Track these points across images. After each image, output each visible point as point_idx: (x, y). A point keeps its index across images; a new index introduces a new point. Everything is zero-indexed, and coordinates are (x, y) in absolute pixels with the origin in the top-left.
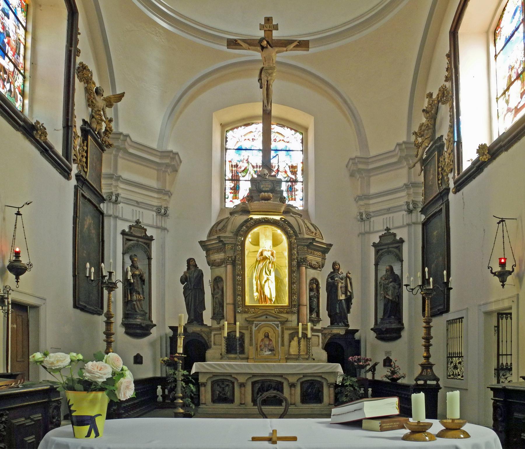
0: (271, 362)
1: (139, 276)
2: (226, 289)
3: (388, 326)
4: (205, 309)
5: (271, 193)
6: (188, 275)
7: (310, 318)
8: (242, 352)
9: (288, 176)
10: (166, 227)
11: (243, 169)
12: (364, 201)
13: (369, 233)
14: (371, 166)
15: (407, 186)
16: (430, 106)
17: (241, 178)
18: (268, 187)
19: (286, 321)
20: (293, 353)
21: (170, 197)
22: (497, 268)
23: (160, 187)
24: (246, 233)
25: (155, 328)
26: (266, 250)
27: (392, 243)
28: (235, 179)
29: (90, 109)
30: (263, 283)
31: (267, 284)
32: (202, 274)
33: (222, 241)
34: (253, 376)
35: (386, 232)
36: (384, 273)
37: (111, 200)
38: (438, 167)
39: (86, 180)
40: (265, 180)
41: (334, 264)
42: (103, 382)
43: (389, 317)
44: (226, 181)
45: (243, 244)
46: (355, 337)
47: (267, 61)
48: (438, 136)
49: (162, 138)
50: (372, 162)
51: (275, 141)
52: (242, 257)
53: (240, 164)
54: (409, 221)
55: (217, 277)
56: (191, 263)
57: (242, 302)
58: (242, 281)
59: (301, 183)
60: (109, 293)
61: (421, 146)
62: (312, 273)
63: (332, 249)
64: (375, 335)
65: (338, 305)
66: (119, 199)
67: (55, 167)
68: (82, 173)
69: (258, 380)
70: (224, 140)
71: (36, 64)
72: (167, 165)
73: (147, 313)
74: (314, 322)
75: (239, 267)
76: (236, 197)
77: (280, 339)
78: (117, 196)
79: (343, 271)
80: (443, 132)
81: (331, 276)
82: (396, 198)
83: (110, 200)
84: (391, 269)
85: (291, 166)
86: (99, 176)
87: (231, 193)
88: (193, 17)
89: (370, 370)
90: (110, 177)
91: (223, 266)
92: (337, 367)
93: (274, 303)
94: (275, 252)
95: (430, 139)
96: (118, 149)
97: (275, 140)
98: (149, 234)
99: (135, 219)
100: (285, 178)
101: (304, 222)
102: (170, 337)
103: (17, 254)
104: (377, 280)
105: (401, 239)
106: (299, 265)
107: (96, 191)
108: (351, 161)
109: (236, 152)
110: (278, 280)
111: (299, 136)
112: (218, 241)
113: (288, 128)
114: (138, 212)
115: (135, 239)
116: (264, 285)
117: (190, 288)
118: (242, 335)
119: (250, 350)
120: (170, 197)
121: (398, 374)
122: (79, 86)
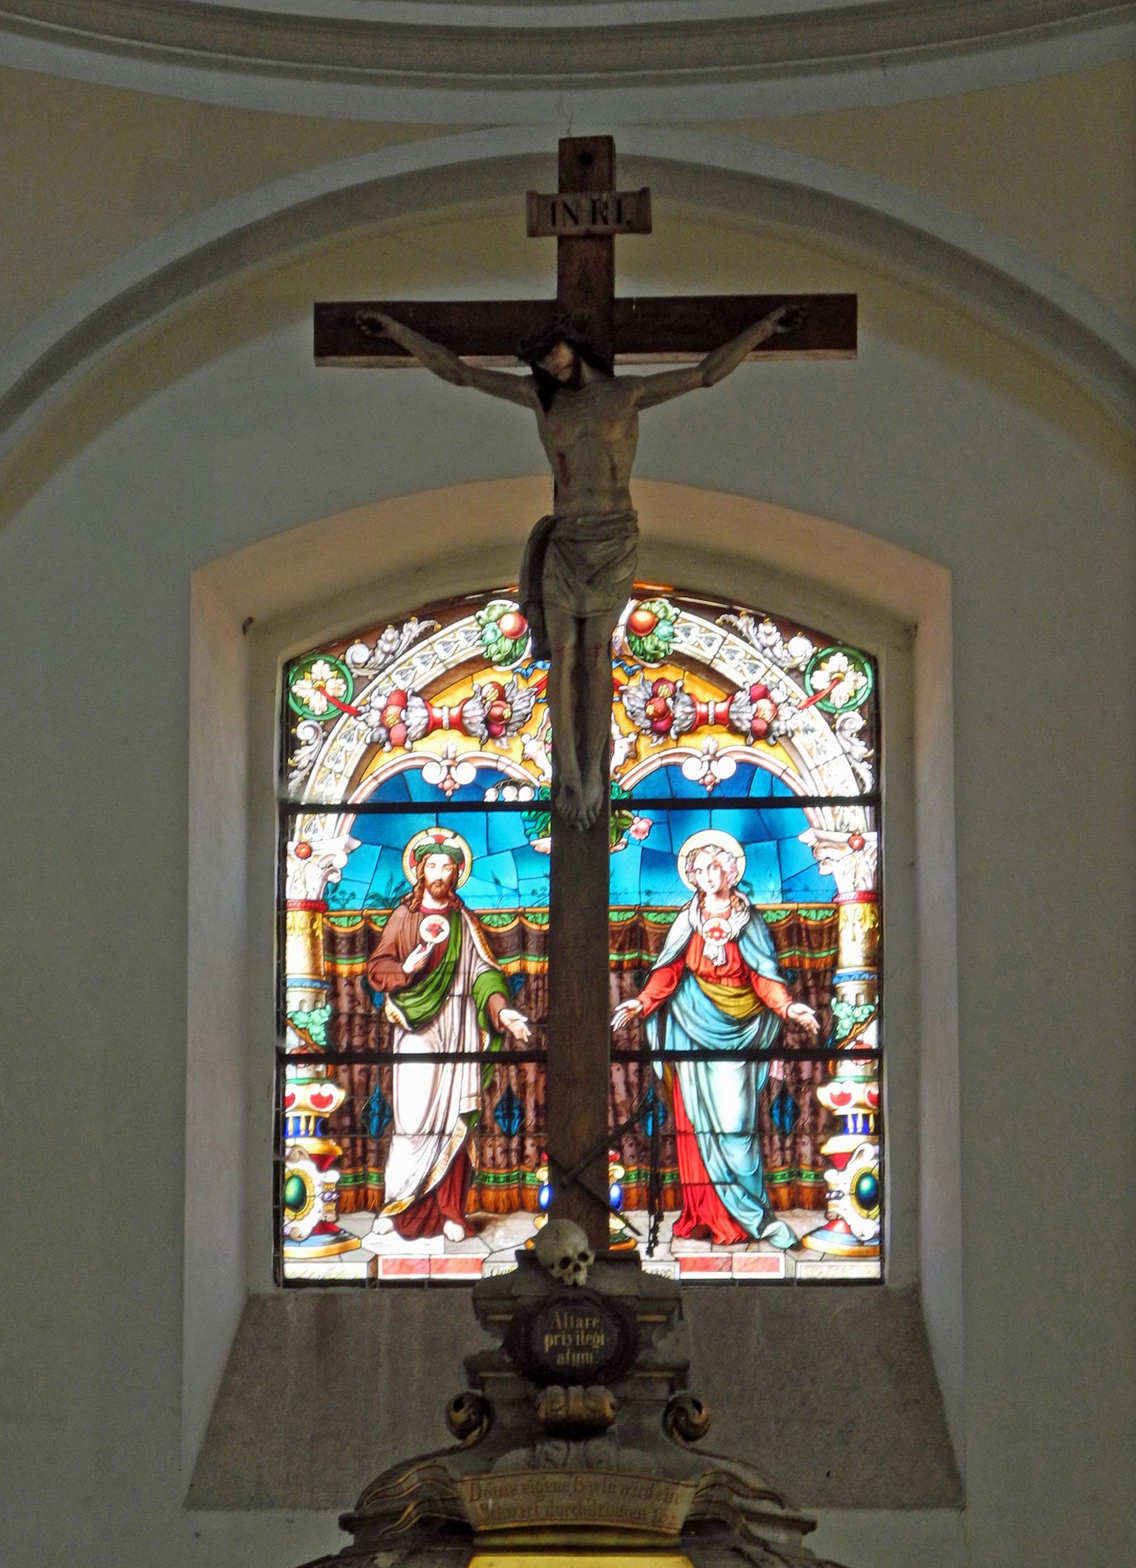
9: (764, 1009)
11: (413, 962)
18: (588, 1348)
40: (571, 1294)
51: (665, 733)
85: (789, 929)
100: (742, 1023)
113: (758, 620)
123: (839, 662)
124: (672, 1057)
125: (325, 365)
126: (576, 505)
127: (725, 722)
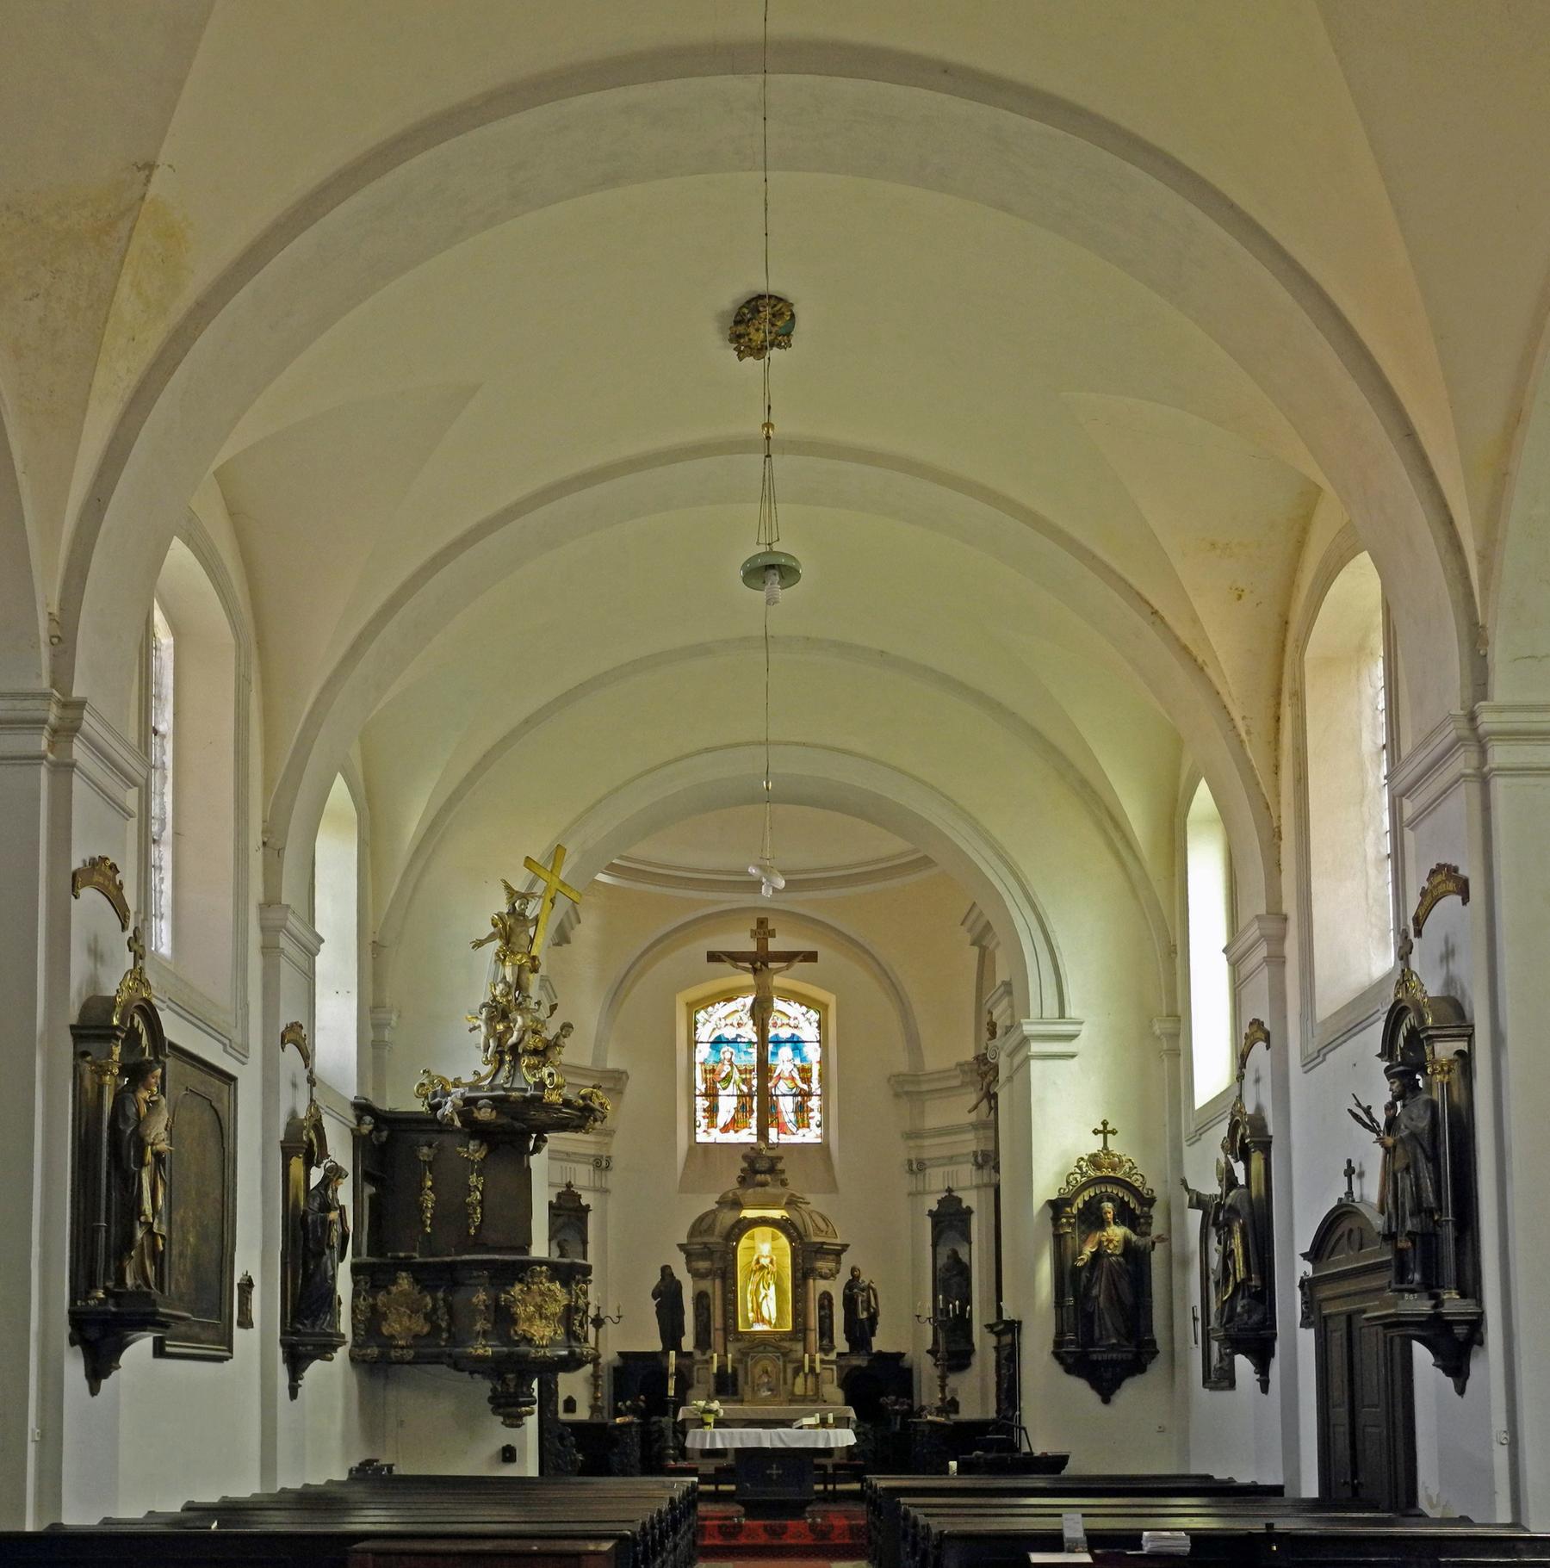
4: (684, 1334)
8: (735, 1393)
9: (797, 1086)
11: (723, 1075)
14: (925, 1087)
17: (721, 1092)
28: (711, 1094)
30: (760, 1300)
31: (765, 1301)
36: (945, 1260)
41: (853, 1270)
56: (666, 1271)
59: (817, 1098)
60: (597, 1331)
62: (821, 1285)
70: (693, 1026)
76: (712, 1125)
77: (782, 1375)
84: (955, 1253)
93: (775, 1327)
94: (775, 1258)
97: (775, 1025)
106: (805, 1277)
111: (813, 1016)
118: (735, 1370)
119: (746, 1391)
123: (812, 1012)
124: (777, 1096)
127: (788, 1024)
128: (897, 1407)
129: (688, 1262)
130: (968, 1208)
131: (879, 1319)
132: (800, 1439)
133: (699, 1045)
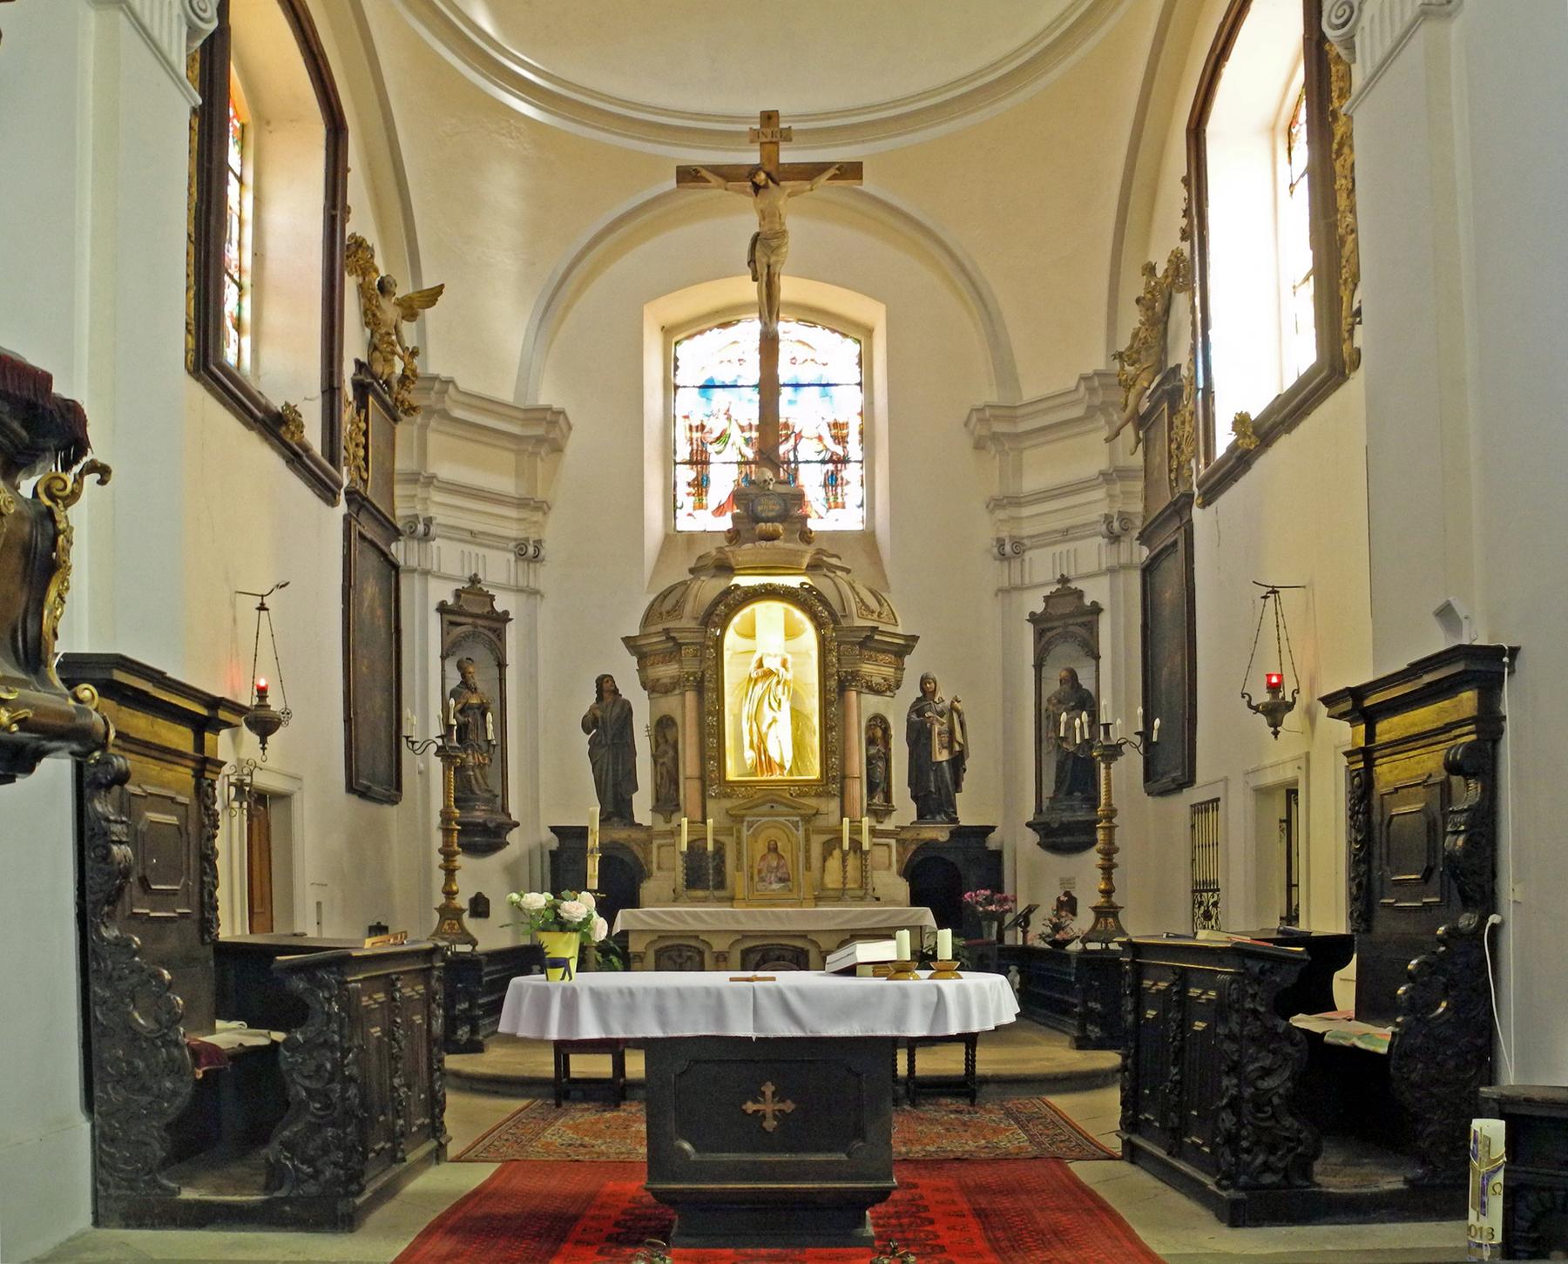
0: (782, 906)
1: (478, 708)
2: (684, 743)
3: (1067, 817)
4: (636, 789)
5: (781, 522)
6: (599, 713)
7: (868, 805)
8: (721, 885)
10: (537, 587)
11: (716, 434)
12: (1007, 511)
13: (1021, 588)
14: (1023, 427)
15: (1107, 477)
16: (1149, 296)
18: (772, 510)
19: (815, 815)
20: (830, 886)
21: (545, 513)
22: (1263, 697)
23: (523, 493)
24: (724, 620)
25: (515, 829)
26: (769, 655)
27: (1071, 615)
28: (699, 460)
29: (368, 331)
32: (630, 710)
33: (674, 639)
34: (744, 937)
35: (1059, 586)
37: (415, 535)
38: (1171, 441)
39: (366, 499)
41: (924, 681)
42: (579, 923)
43: (1070, 793)
44: (678, 466)
45: (719, 643)
46: (987, 845)
47: (767, 220)
48: (1171, 364)
49: (526, 375)
50: (1025, 417)
52: (717, 675)
53: (709, 424)
54: (1113, 562)
55: (665, 716)
56: (605, 685)
57: (719, 772)
58: (718, 726)
61: (1134, 385)
62: (872, 704)
63: (918, 646)
64: (1037, 838)
65: (932, 774)
66: (433, 529)
67: (312, 486)
68: (360, 487)
69: (754, 947)
71: (263, 255)
72: (539, 440)
73: (497, 796)
74: (879, 814)
75: (710, 696)
76: (700, 506)
78: (428, 522)
79: (944, 695)
80: (1180, 355)
81: (918, 708)
82: (1081, 505)
83: (411, 533)
84: (1073, 676)
86: (389, 479)
87: (688, 494)
88: (589, 83)
89: (1016, 923)
90: (413, 478)
91: (677, 692)
92: (923, 916)
95: (1152, 369)
96: (430, 412)
98: (499, 606)
99: (467, 574)
100: (820, 452)
101: (853, 588)
102: (551, 852)
103: (262, 692)
104: (1040, 705)
105: (1094, 604)
106: (842, 688)
107: (384, 516)
108: (974, 414)
109: (700, 393)
110: (797, 716)
111: (851, 349)
112: (664, 638)
114: (473, 555)
115: (470, 620)
116: (766, 734)
117: (603, 742)
118: (720, 849)
119: (736, 879)
120: (545, 513)
121: (1068, 929)
122: (351, 283)
125: (684, 187)
126: (766, 228)
128: (993, 908)
129: (642, 668)
130: (1094, 604)
131: (968, 763)
132: (848, 1008)
133: (680, 391)
